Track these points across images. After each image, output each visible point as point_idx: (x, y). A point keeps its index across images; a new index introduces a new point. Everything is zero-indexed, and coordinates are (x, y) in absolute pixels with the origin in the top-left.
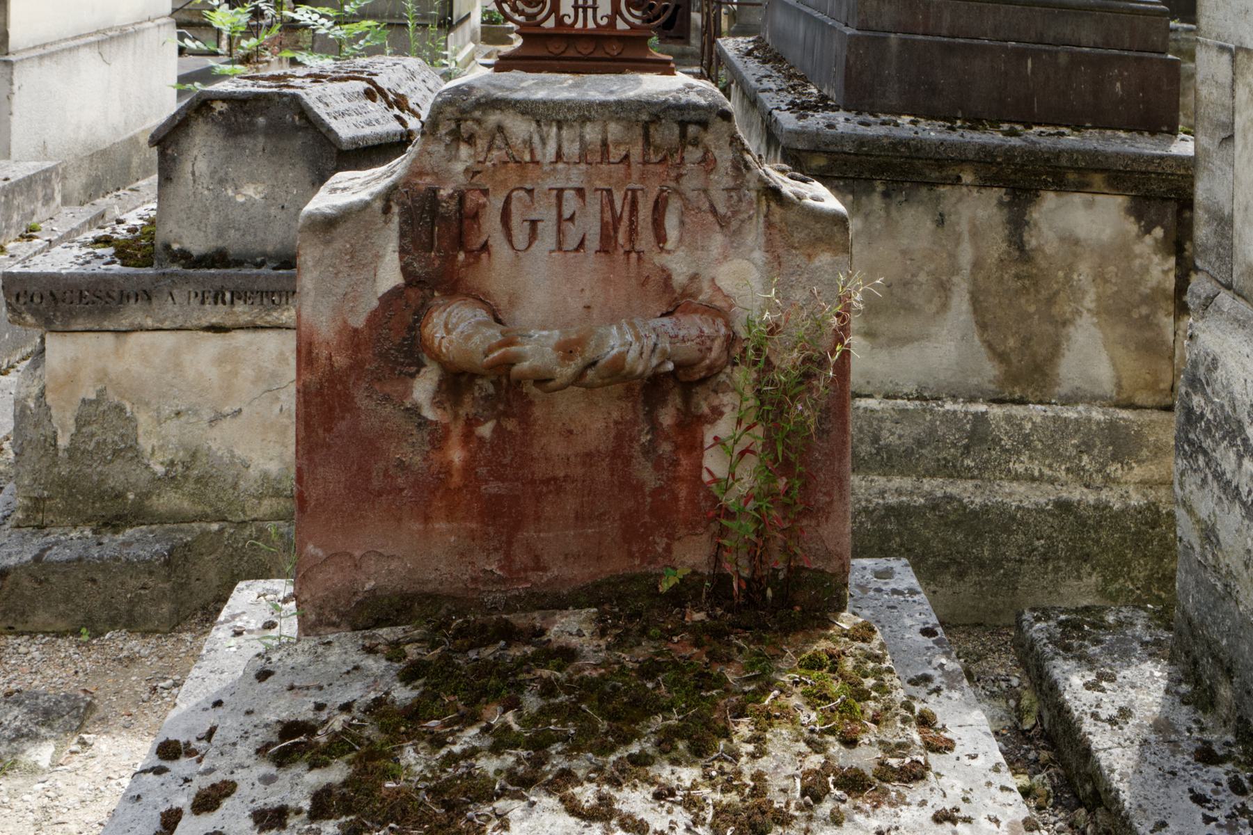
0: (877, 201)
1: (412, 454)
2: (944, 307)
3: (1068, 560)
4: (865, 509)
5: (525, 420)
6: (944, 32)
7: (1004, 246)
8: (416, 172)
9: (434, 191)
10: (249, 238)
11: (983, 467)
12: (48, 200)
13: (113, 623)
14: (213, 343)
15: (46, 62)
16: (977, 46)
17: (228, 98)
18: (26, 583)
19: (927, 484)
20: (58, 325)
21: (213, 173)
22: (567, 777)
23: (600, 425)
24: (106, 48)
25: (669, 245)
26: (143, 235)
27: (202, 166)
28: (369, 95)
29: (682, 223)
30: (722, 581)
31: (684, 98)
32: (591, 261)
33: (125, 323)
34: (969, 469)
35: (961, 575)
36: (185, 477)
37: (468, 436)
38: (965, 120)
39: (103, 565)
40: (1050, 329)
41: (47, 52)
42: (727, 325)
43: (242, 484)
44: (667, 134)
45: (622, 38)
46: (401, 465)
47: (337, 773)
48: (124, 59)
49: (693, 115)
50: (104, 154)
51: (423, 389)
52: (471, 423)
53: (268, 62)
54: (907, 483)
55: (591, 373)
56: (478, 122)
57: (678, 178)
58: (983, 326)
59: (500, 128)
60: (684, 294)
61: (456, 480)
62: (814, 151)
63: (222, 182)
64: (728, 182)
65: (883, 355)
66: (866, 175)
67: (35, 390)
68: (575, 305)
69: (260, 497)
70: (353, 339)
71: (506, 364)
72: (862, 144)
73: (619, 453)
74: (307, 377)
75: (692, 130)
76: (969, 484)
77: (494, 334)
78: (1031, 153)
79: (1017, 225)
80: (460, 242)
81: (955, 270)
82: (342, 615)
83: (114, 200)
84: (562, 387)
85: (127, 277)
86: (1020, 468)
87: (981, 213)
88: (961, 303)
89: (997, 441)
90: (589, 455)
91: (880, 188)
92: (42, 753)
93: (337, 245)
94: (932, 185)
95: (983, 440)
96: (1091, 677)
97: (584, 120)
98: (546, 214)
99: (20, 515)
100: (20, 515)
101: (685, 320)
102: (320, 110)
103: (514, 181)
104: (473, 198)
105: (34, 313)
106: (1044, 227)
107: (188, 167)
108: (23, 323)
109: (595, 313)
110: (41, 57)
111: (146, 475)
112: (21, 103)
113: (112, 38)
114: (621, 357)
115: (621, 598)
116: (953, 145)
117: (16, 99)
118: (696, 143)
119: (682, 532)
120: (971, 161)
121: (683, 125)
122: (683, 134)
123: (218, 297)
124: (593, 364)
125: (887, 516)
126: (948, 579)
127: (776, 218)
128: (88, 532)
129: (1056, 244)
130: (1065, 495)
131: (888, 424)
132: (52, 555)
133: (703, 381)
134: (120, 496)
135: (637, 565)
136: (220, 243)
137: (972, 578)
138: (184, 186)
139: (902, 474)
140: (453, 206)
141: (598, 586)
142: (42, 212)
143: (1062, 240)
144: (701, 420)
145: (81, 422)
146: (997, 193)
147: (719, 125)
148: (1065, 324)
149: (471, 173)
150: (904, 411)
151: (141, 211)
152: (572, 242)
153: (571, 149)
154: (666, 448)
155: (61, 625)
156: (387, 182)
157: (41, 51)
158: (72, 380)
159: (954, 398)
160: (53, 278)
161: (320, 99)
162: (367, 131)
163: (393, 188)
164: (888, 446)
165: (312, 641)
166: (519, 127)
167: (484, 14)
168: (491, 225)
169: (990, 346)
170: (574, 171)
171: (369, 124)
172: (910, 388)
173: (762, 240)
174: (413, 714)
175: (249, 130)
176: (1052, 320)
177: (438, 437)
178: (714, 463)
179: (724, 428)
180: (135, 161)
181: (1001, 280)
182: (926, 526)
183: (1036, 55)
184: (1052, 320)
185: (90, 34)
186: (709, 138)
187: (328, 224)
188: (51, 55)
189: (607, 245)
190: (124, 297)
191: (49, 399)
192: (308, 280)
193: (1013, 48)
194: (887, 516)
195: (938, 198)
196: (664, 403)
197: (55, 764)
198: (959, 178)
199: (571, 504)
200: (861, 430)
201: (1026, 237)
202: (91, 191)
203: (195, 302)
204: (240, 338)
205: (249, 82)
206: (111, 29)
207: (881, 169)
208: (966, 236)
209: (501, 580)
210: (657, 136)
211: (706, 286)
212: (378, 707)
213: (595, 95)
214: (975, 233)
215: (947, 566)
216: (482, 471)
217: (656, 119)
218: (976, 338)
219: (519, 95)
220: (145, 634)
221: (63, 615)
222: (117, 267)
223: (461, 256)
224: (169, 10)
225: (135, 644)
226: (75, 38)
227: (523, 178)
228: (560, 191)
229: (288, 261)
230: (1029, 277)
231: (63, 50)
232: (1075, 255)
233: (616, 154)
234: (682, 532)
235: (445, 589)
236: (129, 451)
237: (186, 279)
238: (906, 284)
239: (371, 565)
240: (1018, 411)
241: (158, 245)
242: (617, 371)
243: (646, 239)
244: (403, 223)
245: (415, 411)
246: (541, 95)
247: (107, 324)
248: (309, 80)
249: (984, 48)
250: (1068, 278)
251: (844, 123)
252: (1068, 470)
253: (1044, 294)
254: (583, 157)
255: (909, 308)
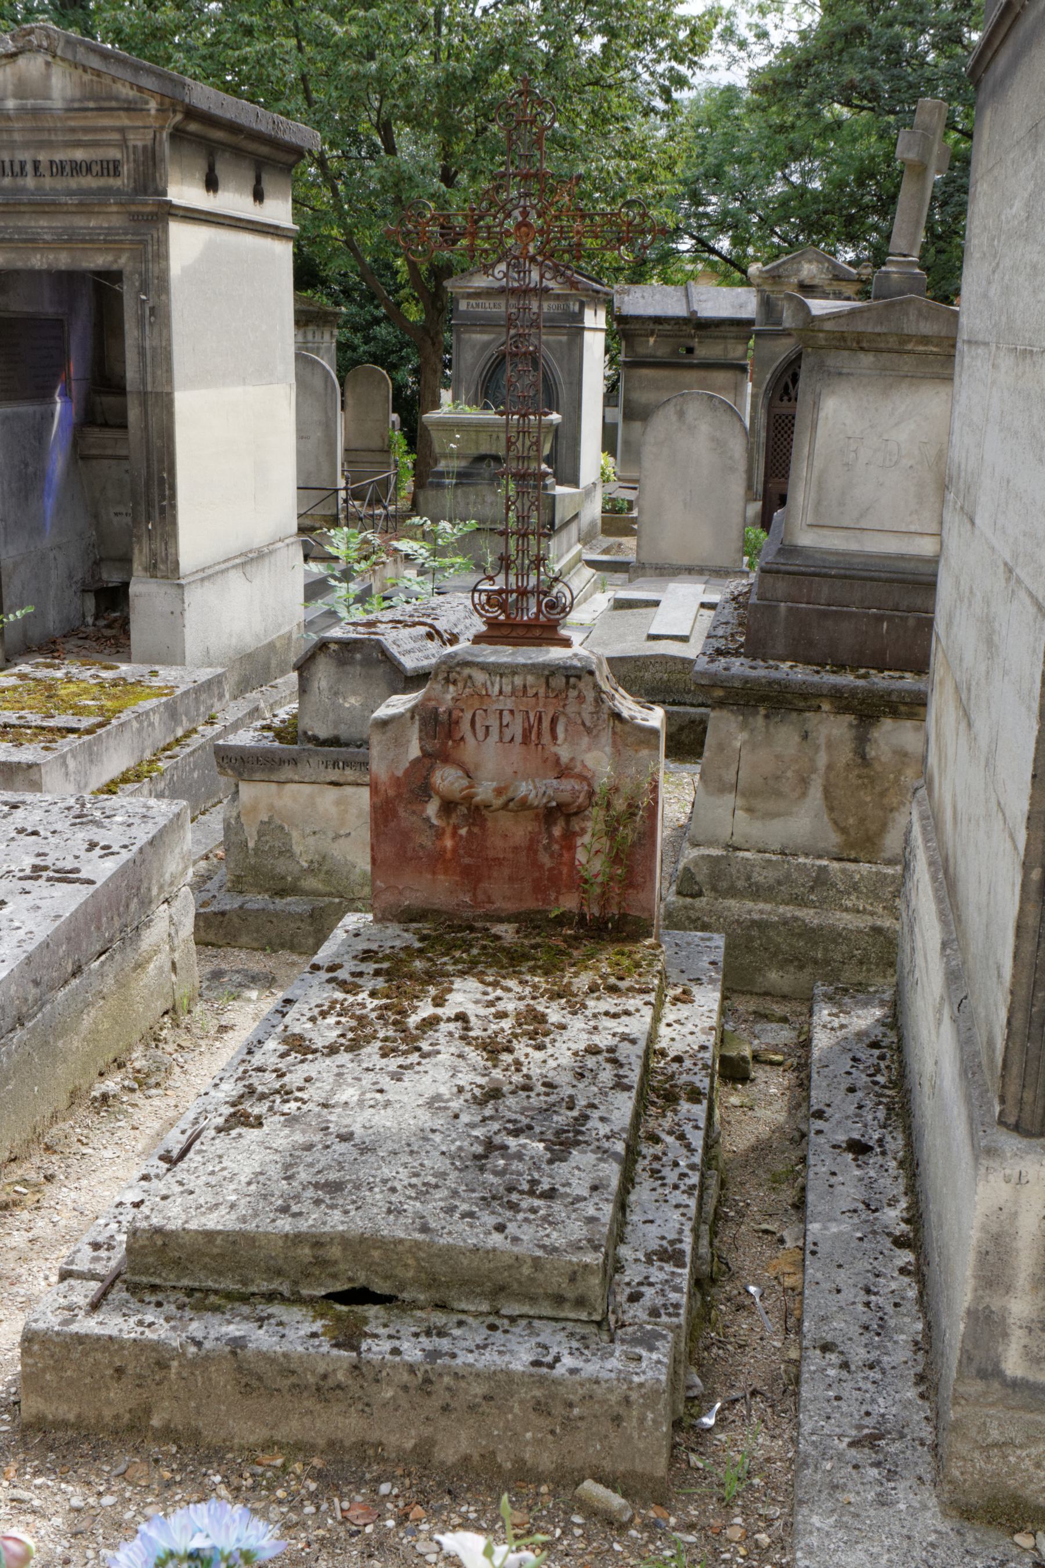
0: (760, 721)
1: (425, 840)
2: (804, 794)
3: (877, 965)
4: (737, 921)
5: (483, 827)
6: (823, 601)
7: (851, 755)
8: (427, 699)
9: (437, 709)
10: (353, 730)
11: (823, 901)
12: (221, 696)
13: (283, 946)
14: (333, 793)
15: (206, 583)
16: (847, 612)
17: (339, 642)
18: (236, 920)
19: (781, 909)
20: (245, 776)
21: (331, 688)
22: (483, 973)
23: (522, 833)
24: (248, 568)
25: (559, 742)
26: (291, 725)
27: (324, 684)
28: (430, 636)
29: (566, 730)
30: (583, 916)
31: (569, 662)
32: (517, 748)
33: (283, 778)
34: (813, 901)
35: (801, 968)
36: (320, 870)
37: (454, 834)
38: (833, 665)
39: (276, 914)
40: (881, 813)
41: (208, 575)
42: (589, 785)
43: (352, 877)
44: (559, 682)
45: (543, 627)
46: (421, 846)
47: (385, 965)
48: (263, 575)
49: (573, 672)
50: (250, 656)
51: (432, 809)
52: (456, 828)
53: (383, 563)
54: (768, 907)
55: (511, 804)
56: (459, 673)
57: (564, 706)
58: (831, 809)
59: (470, 677)
60: (567, 768)
61: (449, 855)
62: (713, 686)
63: (336, 694)
64: (592, 709)
65: (758, 824)
66: (752, 703)
67: (235, 814)
68: (509, 771)
69: (362, 885)
70: (397, 782)
71: (470, 797)
72: (747, 682)
73: (531, 848)
74: (376, 799)
75: (572, 680)
76: (812, 912)
77: (465, 782)
78: (870, 691)
79: (862, 741)
80: (449, 735)
81: (814, 770)
82: (394, 916)
83: (259, 695)
84: (497, 810)
85: (283, 750)
86: (849, 904)
87: (835, 731)
88: (816, 792)
89: (834, 885)
90: (516, 848)
91: (762, 711)
92: (254, 994)
93: (389, 734)
94: (801, 711)
95: (824, 884)
96: (835, 1011)
97: (514, 673)
98: (494, 722)
99: (229, 885)
100: (229, 885)
101: (564, 781)
102: (394, 650)
103: (477, 705)
104: (456, 714)
105: (233, 769)
106: (882, 743)
107: (316, 685)
108: (226, 774)
109: (519, 776)
110: (202, 580)
111: (298, 867)
112: (191, 617)
113: (252, 559)
114: (526, 797)
115: (532, 921)
116: (812, 684)
117: (187, 614)
118: (574, 687)
119: (564, 891)
120: (826, 696)
121: (568, 677)
122: (567, 683)
123: (335, 764)
124: (512, 800)
125: (752, 926)
126: (792, 969)
127: (618, 730)
128: (266, 897)
129: (890, 755)
130: (879, 923)
131: (757, 869)
132: (248, 906)
133: (576, 814)
134: (283, 878)
135: (539, 905)
136: (336, 732)
137: (809, 970)
138: (313, 697)
139: (765, 901)
140: (446, 717)
141: (520, 914)
142: (218, 706)
143: (895, 752)
144: (575, 834)
145: (261, 834)
146: (850, 718)
147: (587, 678)
148: (891, 810)
149: (455, 700)
150: (769, 861)
151: (287, 708)
152: (507, 738)
153: (507, 689)
154: (556, 847)
155: (255, 945)
156: (413, 703)
157: (201, 575)
158: (254, 809)
159: (807, 855)
160: (242, 749)
161: (394, 643)
162: (425, 663)
163: (416, 707)
164: (756, 883)
165: (380, 926)
166: (480, 677)
167: (606, 501)
168: (465, 726)
169: (835, 823)
170: (508, 701)
171: (427, 658)
172: (777, 847)
173: (610, 741)
174: (421, 951)
175: (350, 662)
176: (883, 808)
177: (439, 834)
178: (581, 856)
179: (586, 839)
180: (274, 663)
181: (846, 778)
182: (778, 935)
183: (890, 619)
184: (883, 808)
185: (235, 557)
186: (581, 685)
187: (384, 724)
188: (209, 577)
189: (526, 740)
190: (282, 762)
191: (243, 819)
192: (375, 752)
193: (875, 615)
194: (752, 926)
195: (804, 720)
196: (555, 824)
197: (258, 999)
198: (819, 707)
199: (507, 872)
200: (738, 871)
201: (868, 749)
202: (242, 687)
203: (322, 767)
204: (349, 790)
205: (352, 628)
206: (251, 551)
207: (763, 699)
208: (823, 747)
209: (471, 906)
210: (553, 682)
211: (578, 764)
212: (406, 949)
213: (521, 660)
214: (830, 746)
215: (792, 961)
216: (461, 852)
217: (552, 674)
218: (826, 817)
219: (480, 659)
220: (300, 953)
221: (256, 940)
222: (276, 744)
223: (450, 743)
224: (295, 529)
225: (295, 957)
226: (225, 561)
227: (482, 703)
228: (501, 711)
229: (364, 743)
230: (868, 777)
231: (217, 573)
232: (903, 763)
233: (531, 692)
234: (564, 891)
235: (444, 908)
236: (287, 852)
237: (317, 753)
238: (777, 778)
239: (407, 893)
240: (851, 866)
241: (300, 732)
242: (524, 805)
243: (546, 738)
244: (421, 724)
245: (427, 820)
246: (492, 659)
247: (273, 778)
248: (390, 625)
249: (851, 615)
250: (897, 780)
251: (738, 666)
252: (884, 908)
253: (878, 789)
254: (513, 693)
255: (778, 794)
